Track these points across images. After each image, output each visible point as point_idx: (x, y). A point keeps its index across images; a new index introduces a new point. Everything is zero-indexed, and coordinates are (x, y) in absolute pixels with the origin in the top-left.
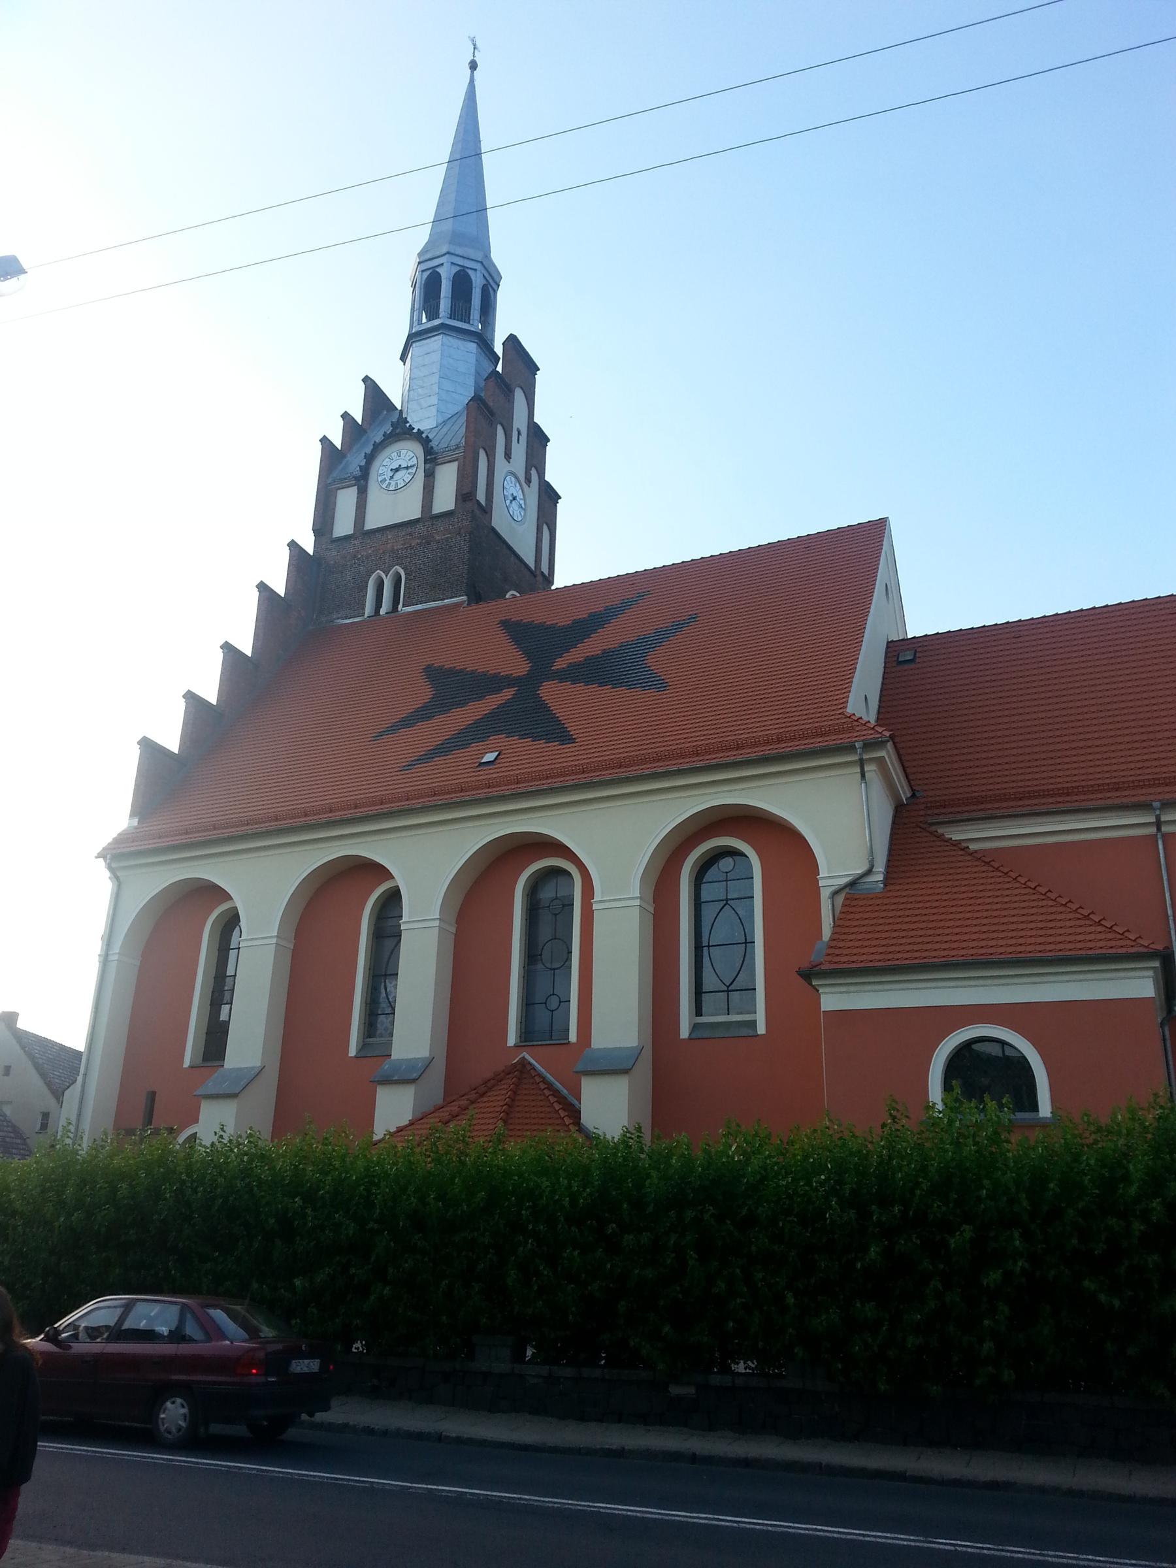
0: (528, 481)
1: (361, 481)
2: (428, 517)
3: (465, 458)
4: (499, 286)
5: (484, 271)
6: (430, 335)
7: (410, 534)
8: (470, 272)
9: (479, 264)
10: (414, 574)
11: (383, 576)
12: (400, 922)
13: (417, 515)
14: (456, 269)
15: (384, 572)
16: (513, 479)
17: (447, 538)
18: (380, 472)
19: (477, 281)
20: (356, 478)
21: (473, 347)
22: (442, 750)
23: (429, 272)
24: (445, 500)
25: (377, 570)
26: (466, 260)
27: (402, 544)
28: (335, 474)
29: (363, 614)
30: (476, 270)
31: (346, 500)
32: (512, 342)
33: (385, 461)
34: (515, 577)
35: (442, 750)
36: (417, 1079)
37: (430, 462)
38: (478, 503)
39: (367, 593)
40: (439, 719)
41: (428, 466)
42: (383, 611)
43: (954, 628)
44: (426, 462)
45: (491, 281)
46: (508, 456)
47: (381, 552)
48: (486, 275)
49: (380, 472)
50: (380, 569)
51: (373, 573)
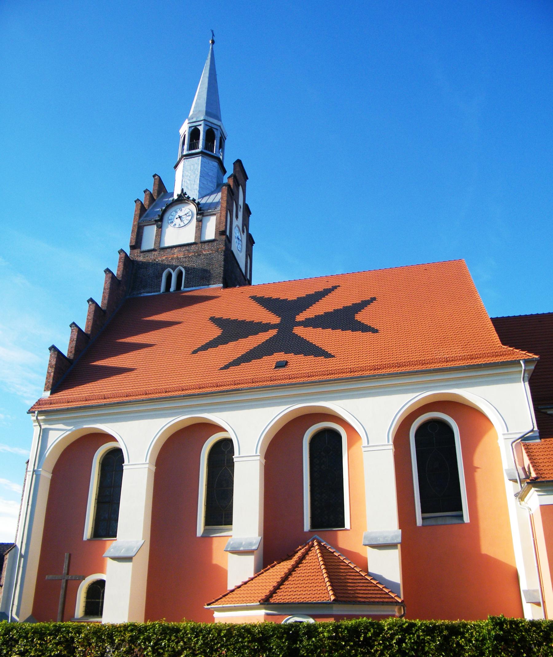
0: (243, 232)
1: (160, 222)
2: (200, 242)
3: (221, 213)
4: (226, 139)
5: (221, 131)
6: (194, 156)
7: (188, 250)
8: (214, 130)
9: (219, 127)
10: (190, 271)
11: (172, 271)
12: (123, 464)
13: (192, 240)
14: (207, 128)
15: (172, 269)
16: (238, 229)
17: (210, 253)
18: (170, 218)
19: (218, 135)
20: (156, 221)
21: (216, 164)
22: (237, 362)
23: (193, 128)
24: (210, 233)
25: (168, 268)
26: (212, 125)
27: (183, 255)
28: (141, 219)
29: (160, 291)
30: (217, 129)
31: (150, 232)
32: (238, 164)
33: (173, 213)
34: (239, 279)
35: (237, 362)
36: (134, 556)
37: (200, 215)
38: (227, 236)
39: (162, 280)
40: (232, 344)
41: (198, 217)
42: (172, 289)
43: (505, 315)
44: (197, 214)
45: (223, 136)
46: (237, 217)
47: (170, 258)
48: (222, 133)
49: (170, 218)
50: (170, 268)
51: (165, 269)
